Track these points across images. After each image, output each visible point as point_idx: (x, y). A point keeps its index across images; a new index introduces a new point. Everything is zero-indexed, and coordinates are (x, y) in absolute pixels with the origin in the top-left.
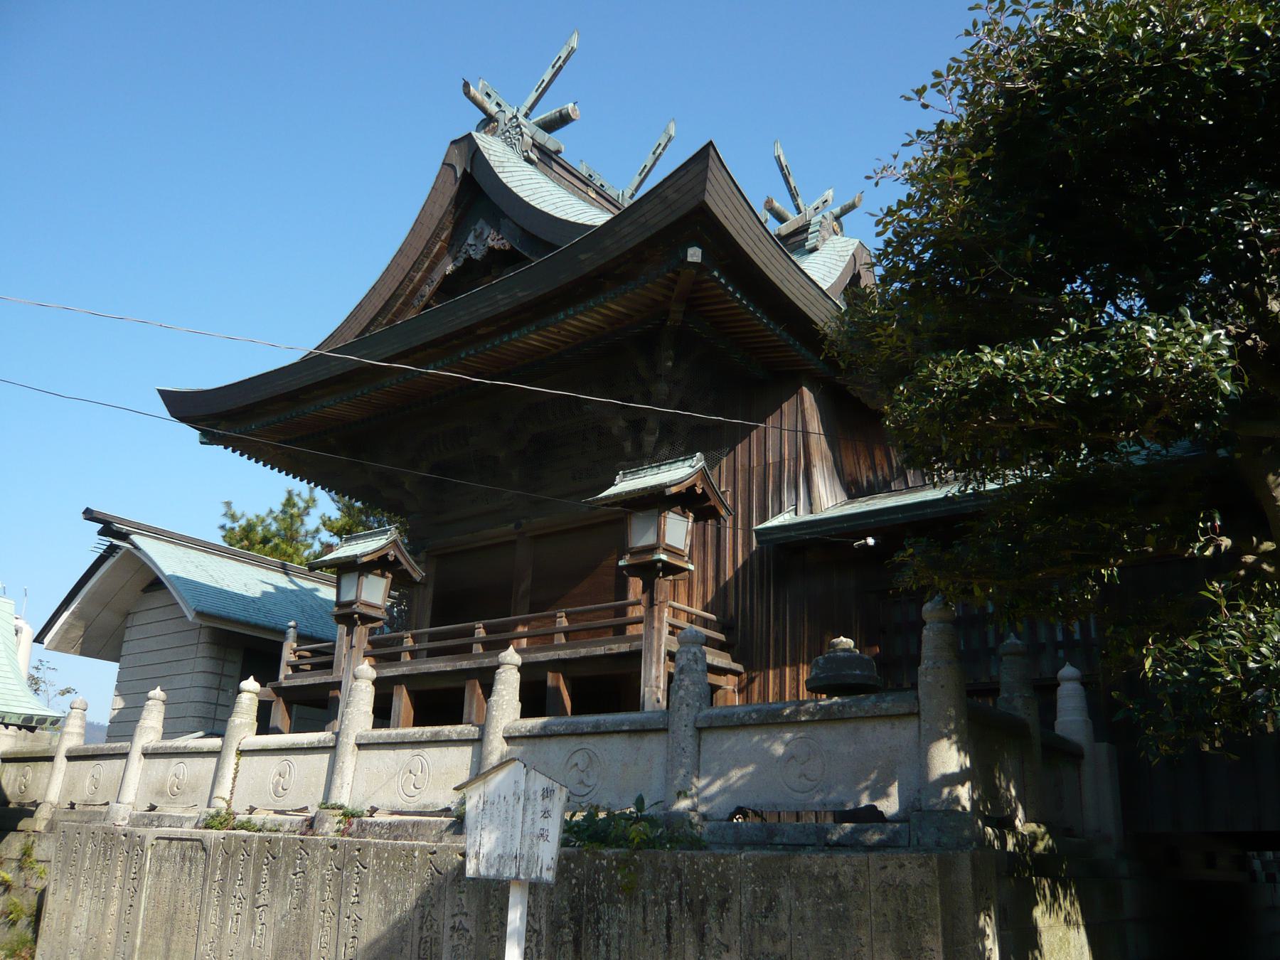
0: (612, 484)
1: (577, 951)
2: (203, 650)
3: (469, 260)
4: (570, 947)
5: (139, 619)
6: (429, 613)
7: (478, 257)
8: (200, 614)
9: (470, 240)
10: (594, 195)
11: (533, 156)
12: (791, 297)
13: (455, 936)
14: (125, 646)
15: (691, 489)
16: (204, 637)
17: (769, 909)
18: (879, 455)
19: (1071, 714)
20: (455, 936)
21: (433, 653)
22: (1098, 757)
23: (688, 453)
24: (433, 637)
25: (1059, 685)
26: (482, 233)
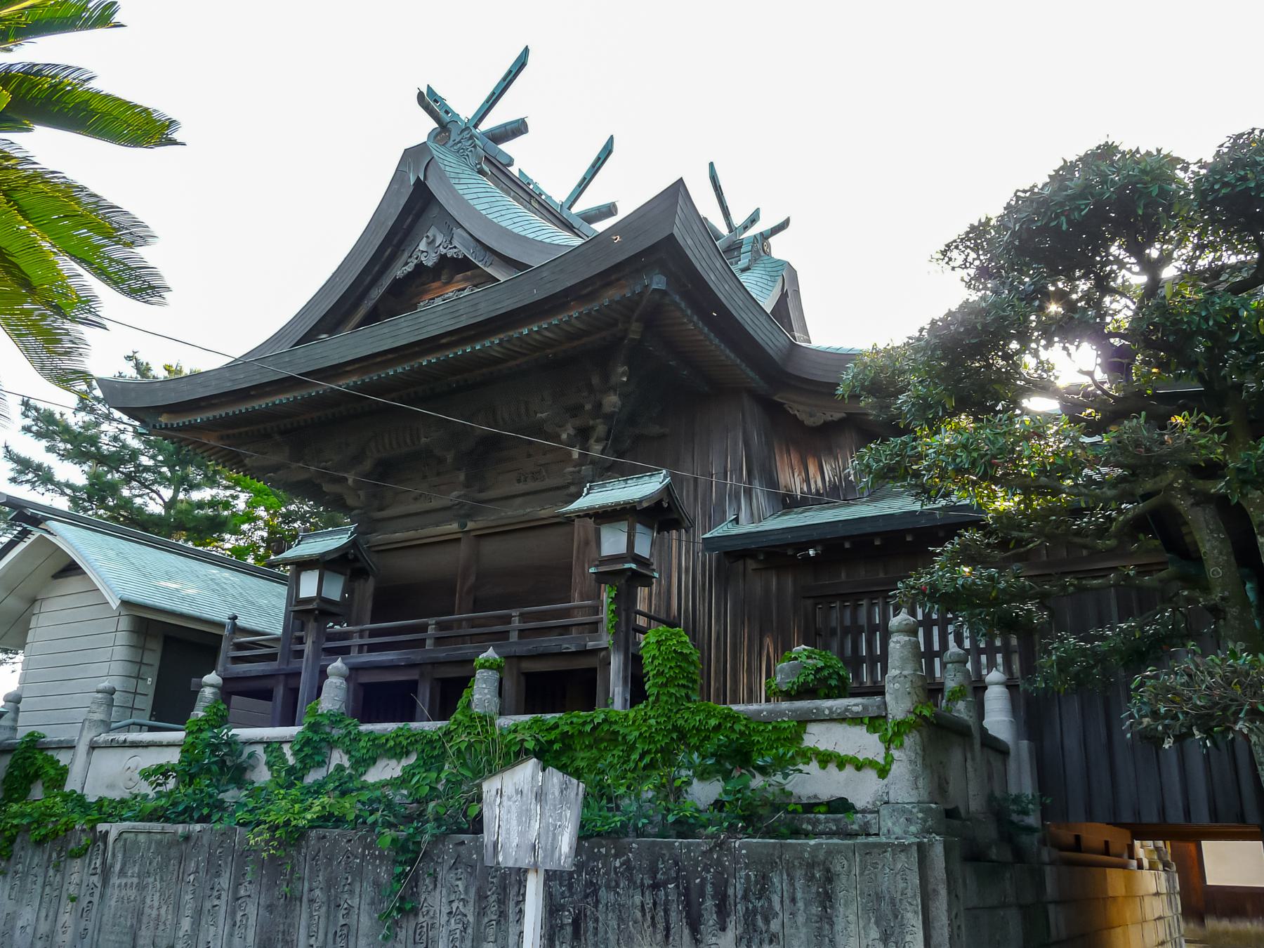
0: (578, 495)
1: (576, 934)
2: (122, 638)
3: (420, 266)
4: (569, 930)
5: (48, 606)
6: (369, 606)
7: (430, 264)
8: (125, 603)
9: (422, 246)
10: (536, 205)
11: (486, 169)
12: (752, 332)
13: (453, 921)
14: (31, 633)
15: (659, 503)
16: (124, 623)
17: (763, 890)
18: (812, 469)
19: (997, 717)
20: (453, 921)
21: (372, 648)
22: (1022, 751)
23: (652, 472)
24: (373, 633)
25: (985, 688)
26: (434, 241)
